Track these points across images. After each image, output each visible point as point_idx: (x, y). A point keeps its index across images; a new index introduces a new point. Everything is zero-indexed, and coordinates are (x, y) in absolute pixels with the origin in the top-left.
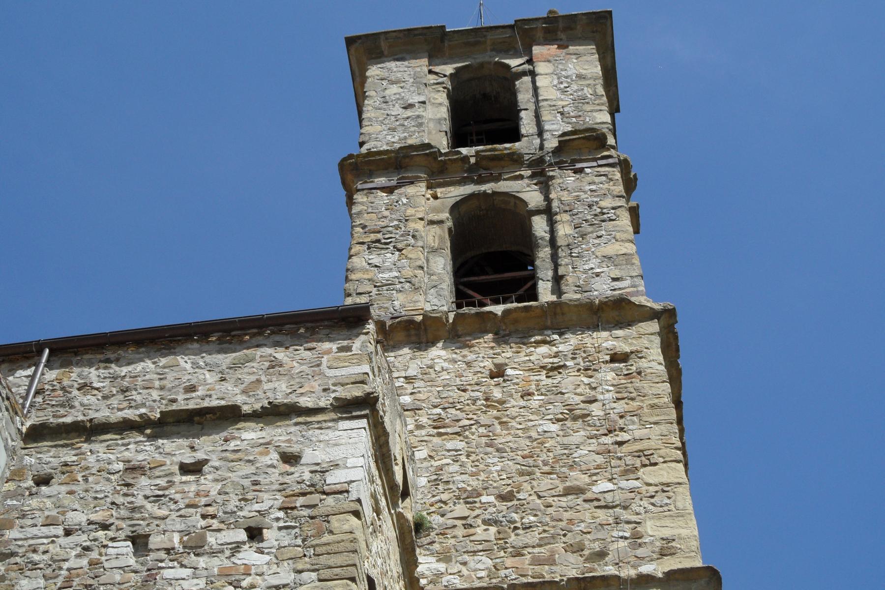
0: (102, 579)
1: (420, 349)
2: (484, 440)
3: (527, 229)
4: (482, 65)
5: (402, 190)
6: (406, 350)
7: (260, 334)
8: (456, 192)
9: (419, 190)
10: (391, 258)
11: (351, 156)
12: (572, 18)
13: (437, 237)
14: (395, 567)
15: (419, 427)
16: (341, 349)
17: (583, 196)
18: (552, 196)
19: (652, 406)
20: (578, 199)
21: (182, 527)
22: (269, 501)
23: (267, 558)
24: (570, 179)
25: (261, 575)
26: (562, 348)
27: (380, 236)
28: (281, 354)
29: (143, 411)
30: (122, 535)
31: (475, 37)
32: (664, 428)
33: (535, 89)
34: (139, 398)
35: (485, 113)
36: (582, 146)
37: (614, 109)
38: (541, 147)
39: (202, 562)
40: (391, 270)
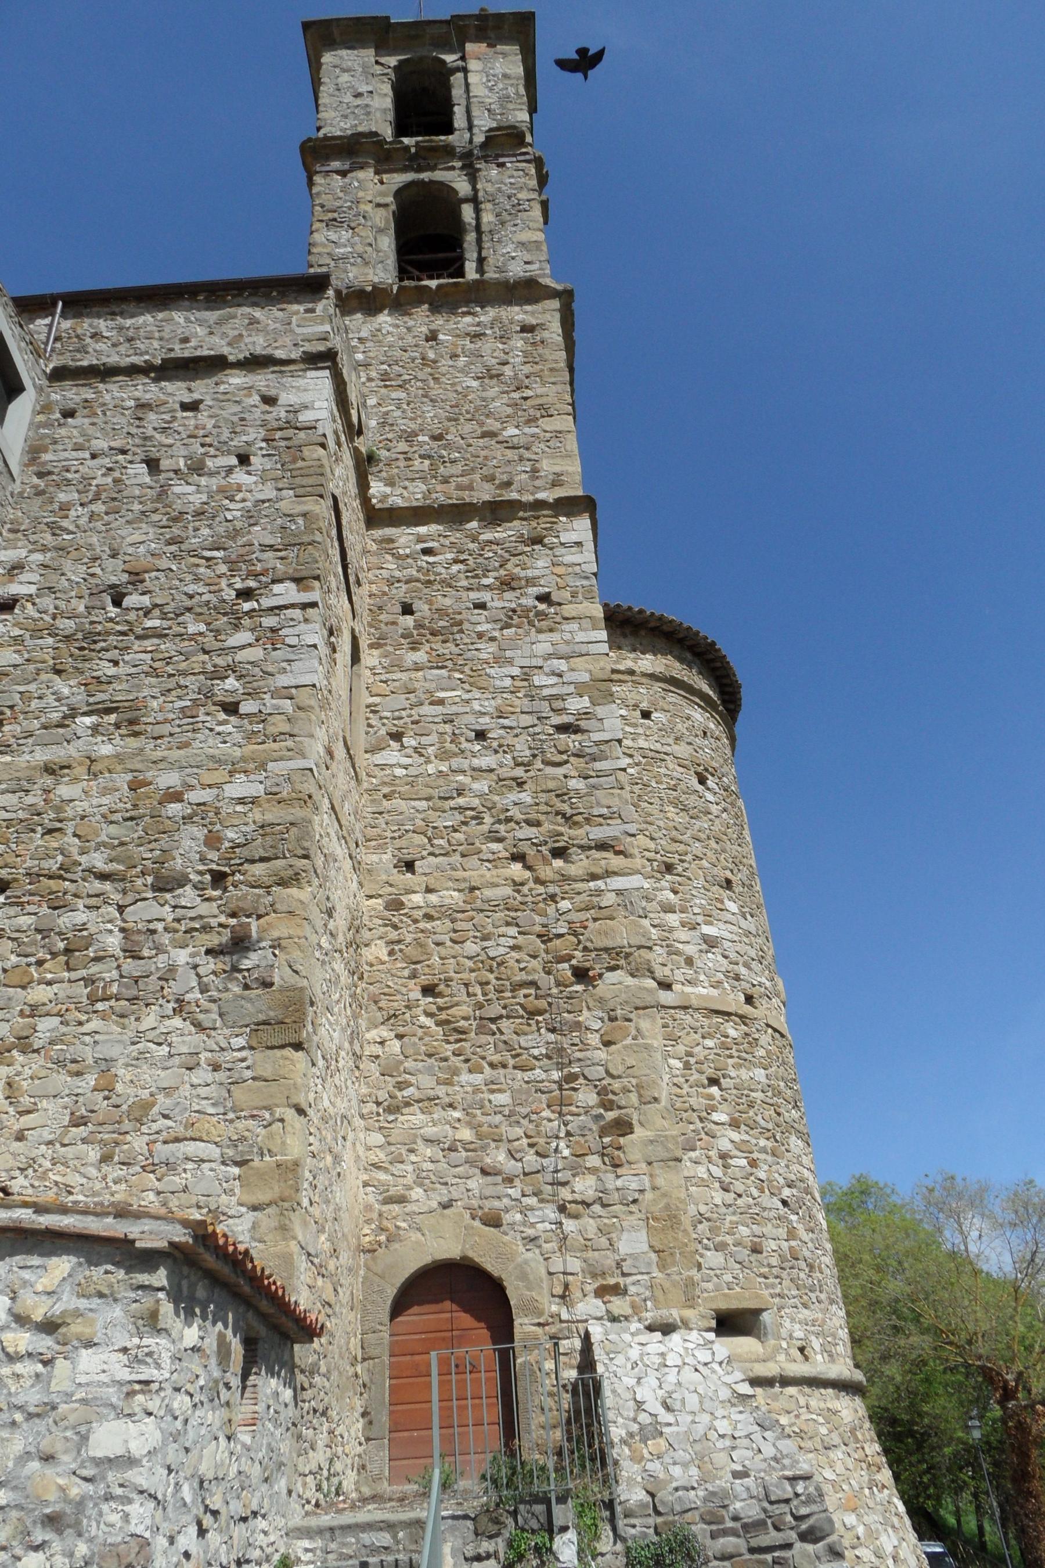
0: (125, 494)
1: (370, 315)
2: (421, 392)
3: (457, 215)
4: (421, 59)
5: (353, 174)
6: (359, 315)
7: (240, 295)
8: (400, 179)
9: (367, 175)
10: (345, 235)
11: (310, 140)
12: (500, 17)
13: (383, 218)
14: (352, 488)
15: (370, 380)
16: (307, 311)
17: (504, 188)
18: (479, 186)
19: (551, 370)
20: (499, 190)
21: (186, 453)
22: (254, 435)
23: (255, 478)
25: (250, 491)
27: (336, 215)
28: (258, 313)
29: (147, 357)
30: (138, 458)
31: (415, 33)
33: (467, 85)
34: (142, 346)
35: (423, 105)
36: (505, 141)
38: (471, 141)
39: (203, 481)
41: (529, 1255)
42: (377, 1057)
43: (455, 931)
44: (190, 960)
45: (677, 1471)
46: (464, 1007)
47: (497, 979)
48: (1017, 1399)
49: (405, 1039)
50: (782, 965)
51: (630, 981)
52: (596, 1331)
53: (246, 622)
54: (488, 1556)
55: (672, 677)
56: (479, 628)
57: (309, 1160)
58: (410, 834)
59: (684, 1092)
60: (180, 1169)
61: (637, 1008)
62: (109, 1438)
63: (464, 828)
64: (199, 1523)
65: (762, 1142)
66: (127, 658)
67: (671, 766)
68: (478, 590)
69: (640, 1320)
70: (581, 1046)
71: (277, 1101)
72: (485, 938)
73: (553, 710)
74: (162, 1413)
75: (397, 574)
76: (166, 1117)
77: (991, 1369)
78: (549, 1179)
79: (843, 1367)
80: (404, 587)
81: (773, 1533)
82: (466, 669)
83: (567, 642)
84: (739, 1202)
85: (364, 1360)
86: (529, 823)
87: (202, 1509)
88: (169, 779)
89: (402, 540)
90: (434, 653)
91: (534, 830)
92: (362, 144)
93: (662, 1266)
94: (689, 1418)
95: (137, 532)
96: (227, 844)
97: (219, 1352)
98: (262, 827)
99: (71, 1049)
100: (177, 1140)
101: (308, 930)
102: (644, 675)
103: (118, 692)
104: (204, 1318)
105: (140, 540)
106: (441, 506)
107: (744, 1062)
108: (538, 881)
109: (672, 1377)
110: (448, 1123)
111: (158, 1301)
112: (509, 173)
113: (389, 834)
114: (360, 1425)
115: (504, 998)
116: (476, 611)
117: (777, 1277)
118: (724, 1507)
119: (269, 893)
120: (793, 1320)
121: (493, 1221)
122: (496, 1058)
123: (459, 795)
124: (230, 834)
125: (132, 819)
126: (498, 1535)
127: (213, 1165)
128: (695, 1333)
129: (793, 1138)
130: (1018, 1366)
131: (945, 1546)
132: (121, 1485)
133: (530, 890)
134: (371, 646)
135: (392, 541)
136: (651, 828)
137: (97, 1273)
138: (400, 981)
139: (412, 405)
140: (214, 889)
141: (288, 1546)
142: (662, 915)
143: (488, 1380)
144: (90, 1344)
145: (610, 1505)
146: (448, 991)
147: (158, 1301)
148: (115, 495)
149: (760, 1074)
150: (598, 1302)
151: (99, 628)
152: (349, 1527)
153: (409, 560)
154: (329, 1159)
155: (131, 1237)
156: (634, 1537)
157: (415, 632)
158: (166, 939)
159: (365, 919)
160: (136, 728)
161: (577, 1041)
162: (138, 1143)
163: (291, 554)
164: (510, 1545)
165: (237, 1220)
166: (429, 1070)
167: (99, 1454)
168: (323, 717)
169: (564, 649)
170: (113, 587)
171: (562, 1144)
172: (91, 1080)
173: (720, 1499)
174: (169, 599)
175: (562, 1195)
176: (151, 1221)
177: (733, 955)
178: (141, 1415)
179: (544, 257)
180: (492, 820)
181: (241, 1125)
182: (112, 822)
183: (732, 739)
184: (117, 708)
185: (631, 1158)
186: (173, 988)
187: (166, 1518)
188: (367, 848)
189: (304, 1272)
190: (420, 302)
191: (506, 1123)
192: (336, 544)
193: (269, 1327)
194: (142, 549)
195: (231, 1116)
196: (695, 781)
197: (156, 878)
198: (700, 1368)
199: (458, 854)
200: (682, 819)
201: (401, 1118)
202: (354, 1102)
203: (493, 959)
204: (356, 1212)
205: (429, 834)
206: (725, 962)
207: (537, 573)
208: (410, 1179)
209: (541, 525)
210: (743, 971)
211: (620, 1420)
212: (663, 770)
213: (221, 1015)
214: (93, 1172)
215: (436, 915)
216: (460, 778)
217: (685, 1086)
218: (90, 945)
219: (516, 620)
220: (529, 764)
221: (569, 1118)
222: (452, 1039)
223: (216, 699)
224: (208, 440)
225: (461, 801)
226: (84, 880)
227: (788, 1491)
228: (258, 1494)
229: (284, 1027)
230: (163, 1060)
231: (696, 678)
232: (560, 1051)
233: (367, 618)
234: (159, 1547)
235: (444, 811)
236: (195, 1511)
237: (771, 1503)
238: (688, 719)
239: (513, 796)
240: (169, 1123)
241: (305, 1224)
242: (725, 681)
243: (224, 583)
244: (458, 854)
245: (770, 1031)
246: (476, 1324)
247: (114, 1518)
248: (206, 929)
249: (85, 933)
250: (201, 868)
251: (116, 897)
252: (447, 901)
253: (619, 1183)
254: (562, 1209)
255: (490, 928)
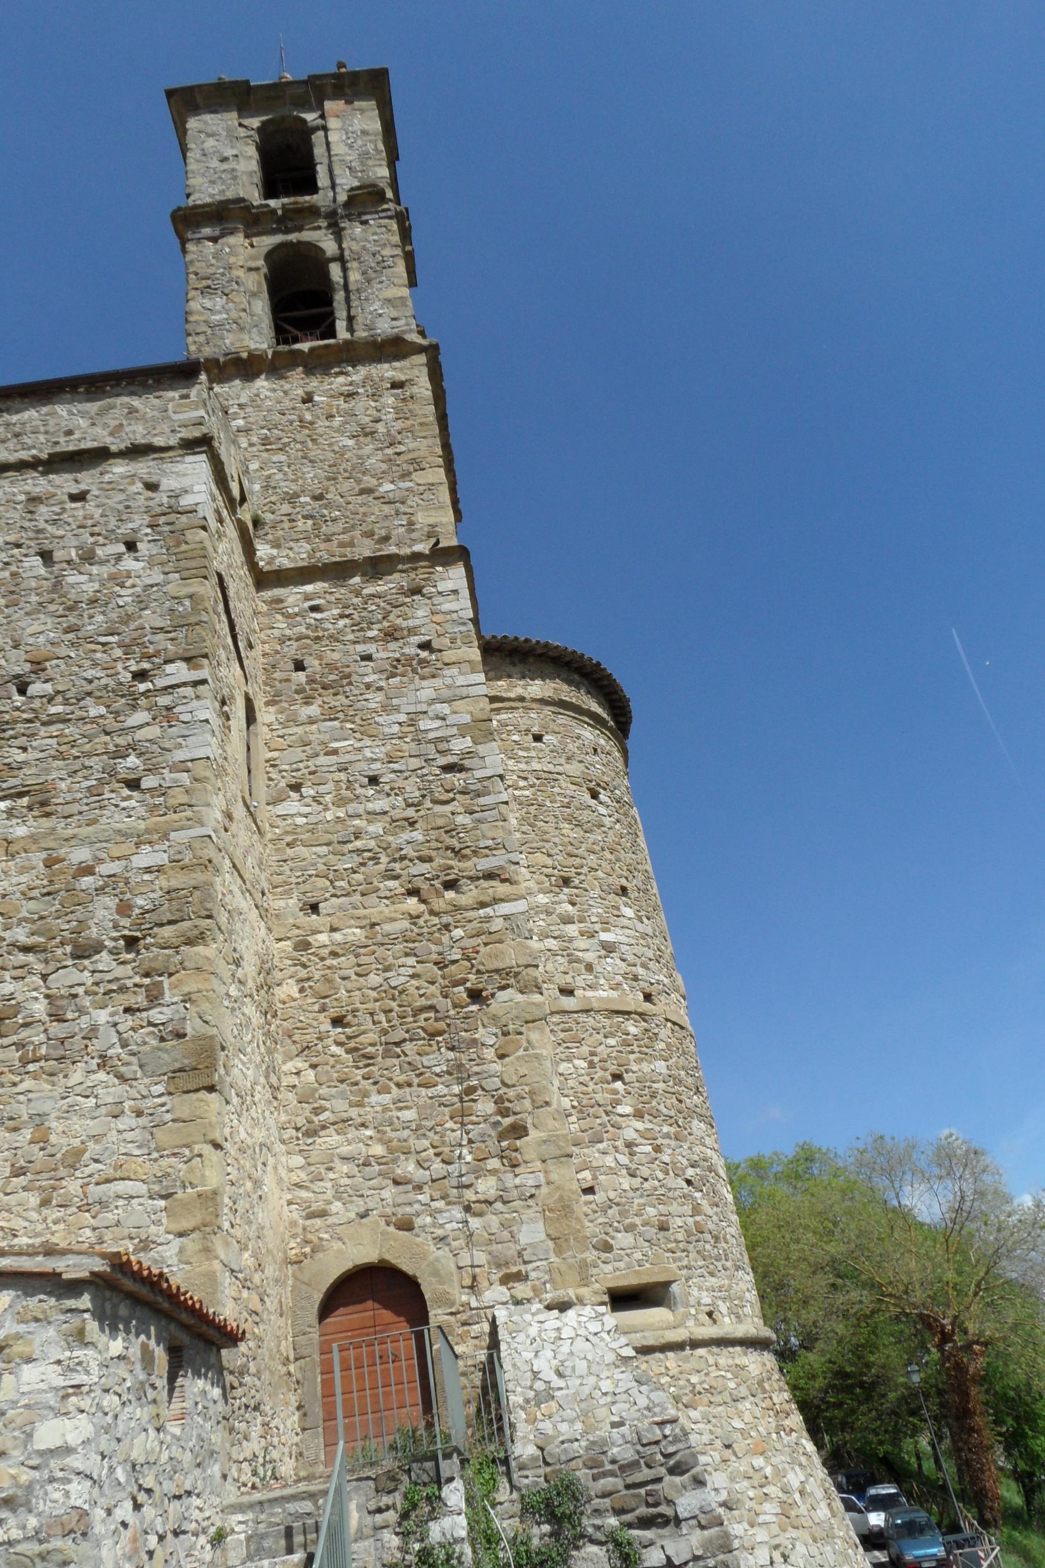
0: (22, 586)
1: (248, 381)
2: (300, 454)
3: (326, 274)
4: (283, 119)
5: (225, 240)
6: (237, 382)
7: (118, 385)
8: (268, 242)
9: (238, 240)
10: (220, 301)
11: (180, 209)
12: (355, 75)
13: (256, 282)
14: (239, 557)
15: (251, 445)
16: (182, 397)
17: (368, 245)
18: (344, 245)
19: (421, 424)
20: (364, 248)
21: (77, 543)
22: (139, 522)
23: (142, 564)
24: (358, 230)
25: (139, 577)
26: (354, 378)
27: (209, 282)
28: (136, 402)
29: (34, 452)
30: (32, 551)
31: (275, 94)
32: (430, 441)
33: (328, 144)
34: (28, 441)
35: (288, 164)
36: (366, 200)
37: (393, 157)
38: (335, 200)
39: (95, 570)
40: (220, 313)
41: (440, 1253)
42: (294, 1087)
43: (359, 965)
44: (110, 1019)
45: (564, 1427)
46: (371, 1035)
47: (400, 1006)
48: (954, 1341)
49: (319, 1068)
50: (681, 961)
51: (520, 998)
52: (501, 1314)
53: (143, 702)
54: (388, 1508)
55: (561, 700)
56: (367, 680)
57: (228, 1188)
58: (314, 879)
59: (590, 1089)
60: (112, 1207)
61: (527, 1022)
62: (49, 1434)
63: (363, 869)
64: (134, 1499)
65: (666, 1129)
66: (34, 744)
67: (564, 785)
68: (364, 642)
69: (540, 1301)
70: (478, 1061)
71: (196, 1139)
72: (386, 970)
73: (438, 752)
74: (93, 1410)
75: (288, 632)
76: (96, 1161)
77: (929, 1316)
78: (455, 1183)
79: (753, 1326)
80: (295, 644)
81: (646, 1470)
82: (357, 719)
83: (449, 687)
84: (646, 1185)
85: (296, 1359)
86: (423, 859)
87: (136, 1488)
88: (81, 855)
89: (291, 600)
90: (326, 706)
91: (427, 865)
92: (230, 210)
93: (558, 1252)
94: (578, 1381)
95: (36, 623)
96: (137, 911)
97: (143, 1359)
98: (168, 892)
99: (8, 1107)
100: (108, 1181)
101: (215, 983)
102: (534, 700)
103: (28, 777)
104: (127, 1331)
105: (40, 631)
106: (325, 564)
107: (646, 1056)
108: (432, 913)
109: (565, 1348)
110: (361, 1141)
111: (84, 1320)
112: (372, 230)
113: (294, 880)
114: (296, 1418)
115: (406, 1023)
116: (363, 663)
117: (683, 1251)
118: (604, 1453)
119: (178, 953)
120: (700, 1288)
121: (406, 1226)
122: (401, 1079)
123: (356, 838)
124: (140, 901)
125: (49, 894)
126: (395, 1490)
127: (141, 1200)
128: (588, 1308)
129: (695, 1122)
130: (951, 1313)
131: (900, 1487)
132: (62, 1470)
133: (426, 922)
134: (267, 704)
135: (281, 601)
136: (548, 845)
137: (32, 1302)
138: (311, 1015)
139: (293, 467)
140: (128, 952)
141: (224, 1520)
142: (562, 926)
143: (408, 1367)
144: (29, 1360)
145: (506, 1462)
146: (356, 1021)
147: (84, 1320)
148: (13, 589)
149: (661, 1066)
150: (504, 1289)
151: (7, 717)
152: (276, 1499)
153: (298, 619)
154: (249, 1185)
155: (58, 1270)
156: (527, 1486)
157: (308, 687)
158: (87, 1001)
159: (276, 962)
160: (48, 809)
161: (474, 1056)
162: (73, 1186)
163: (180, 634)
164: (405, 1497)
165: (165, 1247)
166: (342, 1095)
167: (42, 1447)
168: (220, 784)
169: (446, 693)
170: (17, 676)
171: (465, 1151)
172: (27, 1134)
173: (600, 1447)
174: (69, 686)
175: (467, 1197)
176: (75, 1256)
177: (630, 958)
178: (74, 1413)
179: (409, 312)
180: (388, 859)
181: (164, 1162)
182: (31, 899)
183: (625, 752)
184: (28, 792)
185: (527, 1158)
186: (95, 1046)
187: (102, 1495)
188: (275, 894)
189: (228, 1287)
190: (293, 366)
191: (413, 1137)
192: (224, 618)
193: (193, 1338)
194: (42, 639)
195: (155, 1155)
196: (587, 797)
197: (75, 947)
198: (591, 1337)
199: (358, 893)
200: (576, 834)
201: (319, 1141)
202: (274, 1131)
203: (395, 988)
204: (282, 1229)
205: (331, 877)
206: (623, 964)
207: (417, 622)
208: (330, 1194)
209: (418, 576)
210: (641, 971)
211: (519, 1389)
212: (556, 790)
213: (141, 1066)
214: (34, 1215)
215: (341, 952)
216: (357, 822)
217: (591, 1084)
218: (19, 1012)
219: (401, 669)
220: (419, 804)
221: (470, 1127)
222: (361, 1064)
223: (119, 777)
224: (96, 529)
225: (358, 844)
226: (9, 953)
227: (658, 1433)
228: (190, 1477)
229: (198, 1070)
230: (89, 1111)
231: (585, 698)
232: (460, 1066)
233: (262, 677)
234: (97, 1518)
235: (343, 855)
236: (129, 1489)
237: (644, 1445)
238: (578, 738)
239: (406, 836)
240: (100, 1166)
241: (227, 1244)
242: (614, 697)
243: (120, 666)
244: (358, 893)
245: (669, 1024)
246: (396, 1319)
247: (58, 1496)
248: (123, 989)
249: (13, 1002)
250: (115, 934)
251: (39, 967)
252: (351, 938)
253: (517, 1181)
254: (467, 1209)
255: (391, 960)
